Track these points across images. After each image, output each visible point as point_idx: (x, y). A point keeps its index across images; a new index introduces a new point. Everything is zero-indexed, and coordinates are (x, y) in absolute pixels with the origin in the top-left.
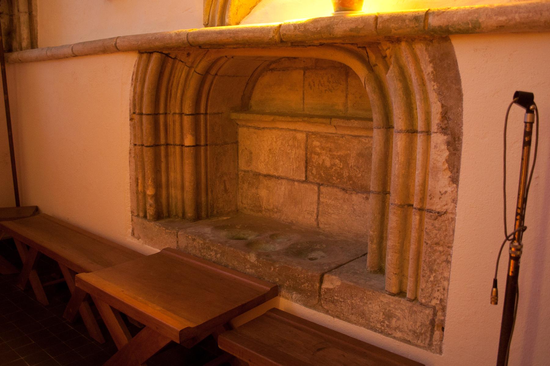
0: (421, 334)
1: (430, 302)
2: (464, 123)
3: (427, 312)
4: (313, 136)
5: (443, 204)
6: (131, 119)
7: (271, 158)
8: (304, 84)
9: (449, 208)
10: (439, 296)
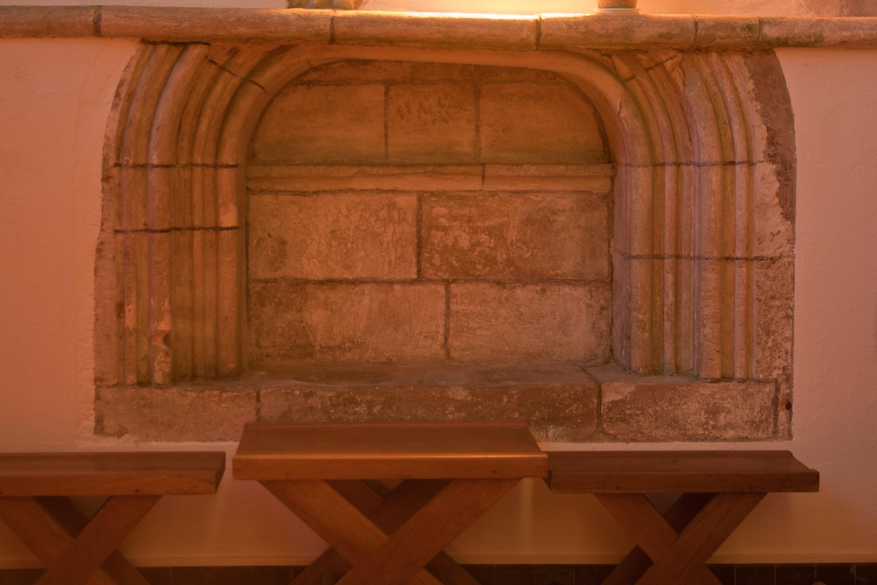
0: (761, 422)
1: (770, 375)
2: (797, 147)
3: (767, 389)
4: (433, 199)
5: (776, 247)
6: (106, 179)
7: (336, 247)
8: (386, 109)
9: (785, 251)
10: (780, 364)
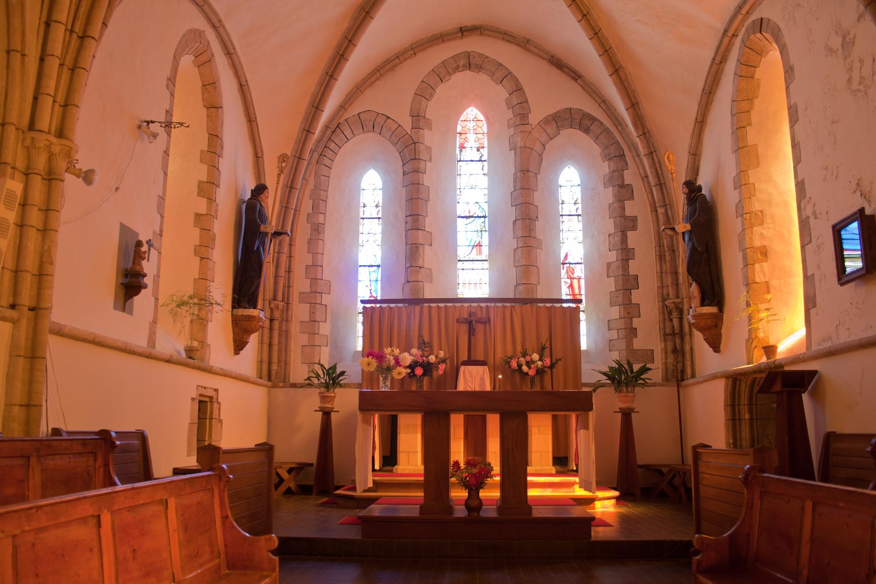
6: (725, 408)
